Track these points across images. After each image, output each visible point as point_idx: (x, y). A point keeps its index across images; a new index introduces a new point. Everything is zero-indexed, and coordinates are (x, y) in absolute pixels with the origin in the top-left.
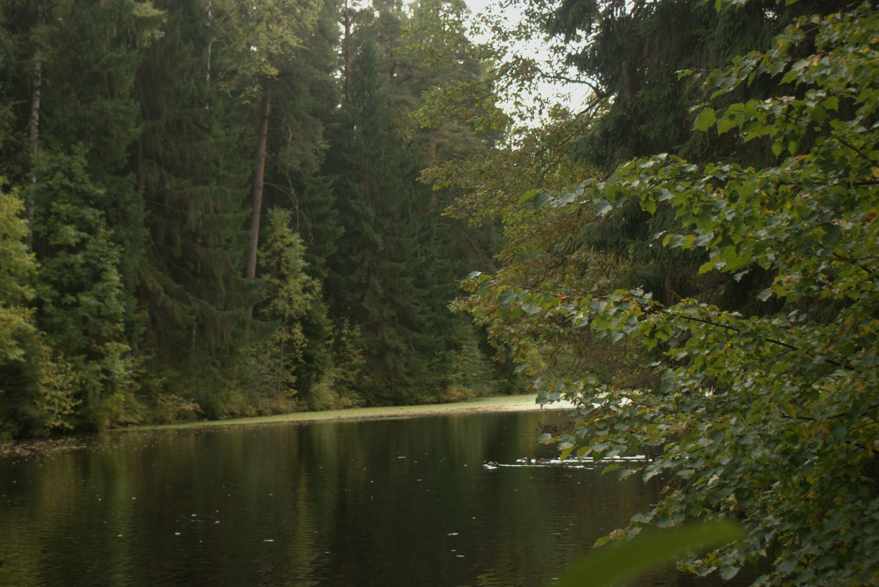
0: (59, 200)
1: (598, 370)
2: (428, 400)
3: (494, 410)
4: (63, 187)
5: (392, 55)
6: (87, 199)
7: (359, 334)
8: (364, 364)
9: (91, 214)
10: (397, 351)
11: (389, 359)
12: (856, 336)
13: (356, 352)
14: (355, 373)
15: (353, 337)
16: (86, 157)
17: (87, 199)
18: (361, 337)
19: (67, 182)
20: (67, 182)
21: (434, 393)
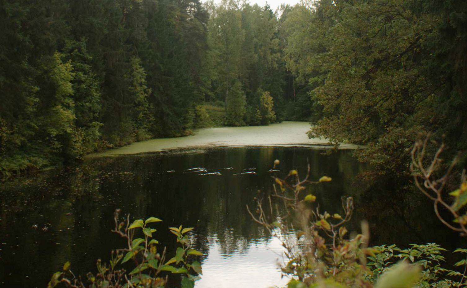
0: (76, 61)
1: (229, 118)
2: (178, 135)
3: (218, 144)
4: (77, 55)
5: (388, 74)
6: (84, 60)
7: (152, 107)
8: (155, 120)
9: (87, 67)
10: (168, 115)
11: (27, 93)
12: (388, 37)
13: (151, 115)
14: (150, 124)
15: (150, 109)
16: (86, 43)
17: (84, 60)
18: (153, 109)
19: (79, 54)
20: (79, 54)
21: (179, 133)
